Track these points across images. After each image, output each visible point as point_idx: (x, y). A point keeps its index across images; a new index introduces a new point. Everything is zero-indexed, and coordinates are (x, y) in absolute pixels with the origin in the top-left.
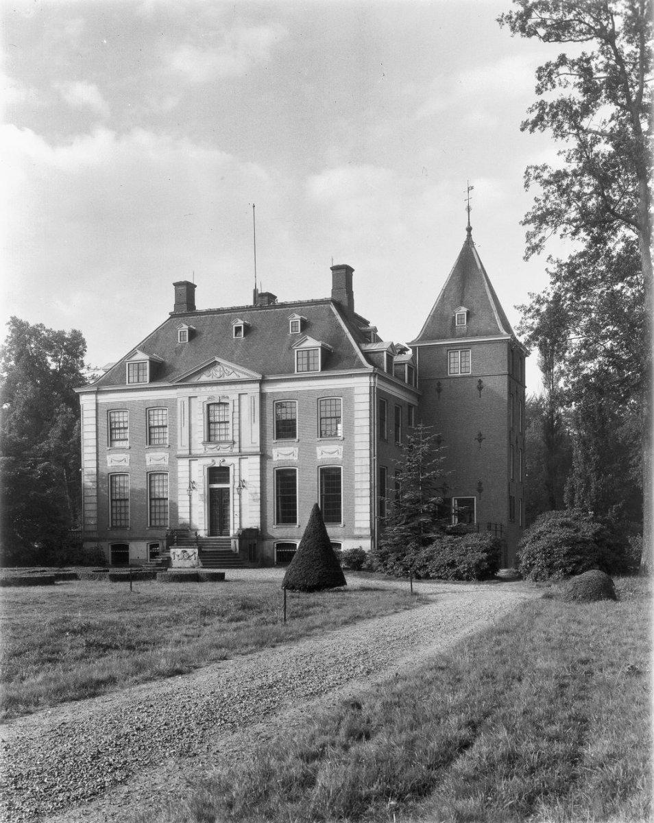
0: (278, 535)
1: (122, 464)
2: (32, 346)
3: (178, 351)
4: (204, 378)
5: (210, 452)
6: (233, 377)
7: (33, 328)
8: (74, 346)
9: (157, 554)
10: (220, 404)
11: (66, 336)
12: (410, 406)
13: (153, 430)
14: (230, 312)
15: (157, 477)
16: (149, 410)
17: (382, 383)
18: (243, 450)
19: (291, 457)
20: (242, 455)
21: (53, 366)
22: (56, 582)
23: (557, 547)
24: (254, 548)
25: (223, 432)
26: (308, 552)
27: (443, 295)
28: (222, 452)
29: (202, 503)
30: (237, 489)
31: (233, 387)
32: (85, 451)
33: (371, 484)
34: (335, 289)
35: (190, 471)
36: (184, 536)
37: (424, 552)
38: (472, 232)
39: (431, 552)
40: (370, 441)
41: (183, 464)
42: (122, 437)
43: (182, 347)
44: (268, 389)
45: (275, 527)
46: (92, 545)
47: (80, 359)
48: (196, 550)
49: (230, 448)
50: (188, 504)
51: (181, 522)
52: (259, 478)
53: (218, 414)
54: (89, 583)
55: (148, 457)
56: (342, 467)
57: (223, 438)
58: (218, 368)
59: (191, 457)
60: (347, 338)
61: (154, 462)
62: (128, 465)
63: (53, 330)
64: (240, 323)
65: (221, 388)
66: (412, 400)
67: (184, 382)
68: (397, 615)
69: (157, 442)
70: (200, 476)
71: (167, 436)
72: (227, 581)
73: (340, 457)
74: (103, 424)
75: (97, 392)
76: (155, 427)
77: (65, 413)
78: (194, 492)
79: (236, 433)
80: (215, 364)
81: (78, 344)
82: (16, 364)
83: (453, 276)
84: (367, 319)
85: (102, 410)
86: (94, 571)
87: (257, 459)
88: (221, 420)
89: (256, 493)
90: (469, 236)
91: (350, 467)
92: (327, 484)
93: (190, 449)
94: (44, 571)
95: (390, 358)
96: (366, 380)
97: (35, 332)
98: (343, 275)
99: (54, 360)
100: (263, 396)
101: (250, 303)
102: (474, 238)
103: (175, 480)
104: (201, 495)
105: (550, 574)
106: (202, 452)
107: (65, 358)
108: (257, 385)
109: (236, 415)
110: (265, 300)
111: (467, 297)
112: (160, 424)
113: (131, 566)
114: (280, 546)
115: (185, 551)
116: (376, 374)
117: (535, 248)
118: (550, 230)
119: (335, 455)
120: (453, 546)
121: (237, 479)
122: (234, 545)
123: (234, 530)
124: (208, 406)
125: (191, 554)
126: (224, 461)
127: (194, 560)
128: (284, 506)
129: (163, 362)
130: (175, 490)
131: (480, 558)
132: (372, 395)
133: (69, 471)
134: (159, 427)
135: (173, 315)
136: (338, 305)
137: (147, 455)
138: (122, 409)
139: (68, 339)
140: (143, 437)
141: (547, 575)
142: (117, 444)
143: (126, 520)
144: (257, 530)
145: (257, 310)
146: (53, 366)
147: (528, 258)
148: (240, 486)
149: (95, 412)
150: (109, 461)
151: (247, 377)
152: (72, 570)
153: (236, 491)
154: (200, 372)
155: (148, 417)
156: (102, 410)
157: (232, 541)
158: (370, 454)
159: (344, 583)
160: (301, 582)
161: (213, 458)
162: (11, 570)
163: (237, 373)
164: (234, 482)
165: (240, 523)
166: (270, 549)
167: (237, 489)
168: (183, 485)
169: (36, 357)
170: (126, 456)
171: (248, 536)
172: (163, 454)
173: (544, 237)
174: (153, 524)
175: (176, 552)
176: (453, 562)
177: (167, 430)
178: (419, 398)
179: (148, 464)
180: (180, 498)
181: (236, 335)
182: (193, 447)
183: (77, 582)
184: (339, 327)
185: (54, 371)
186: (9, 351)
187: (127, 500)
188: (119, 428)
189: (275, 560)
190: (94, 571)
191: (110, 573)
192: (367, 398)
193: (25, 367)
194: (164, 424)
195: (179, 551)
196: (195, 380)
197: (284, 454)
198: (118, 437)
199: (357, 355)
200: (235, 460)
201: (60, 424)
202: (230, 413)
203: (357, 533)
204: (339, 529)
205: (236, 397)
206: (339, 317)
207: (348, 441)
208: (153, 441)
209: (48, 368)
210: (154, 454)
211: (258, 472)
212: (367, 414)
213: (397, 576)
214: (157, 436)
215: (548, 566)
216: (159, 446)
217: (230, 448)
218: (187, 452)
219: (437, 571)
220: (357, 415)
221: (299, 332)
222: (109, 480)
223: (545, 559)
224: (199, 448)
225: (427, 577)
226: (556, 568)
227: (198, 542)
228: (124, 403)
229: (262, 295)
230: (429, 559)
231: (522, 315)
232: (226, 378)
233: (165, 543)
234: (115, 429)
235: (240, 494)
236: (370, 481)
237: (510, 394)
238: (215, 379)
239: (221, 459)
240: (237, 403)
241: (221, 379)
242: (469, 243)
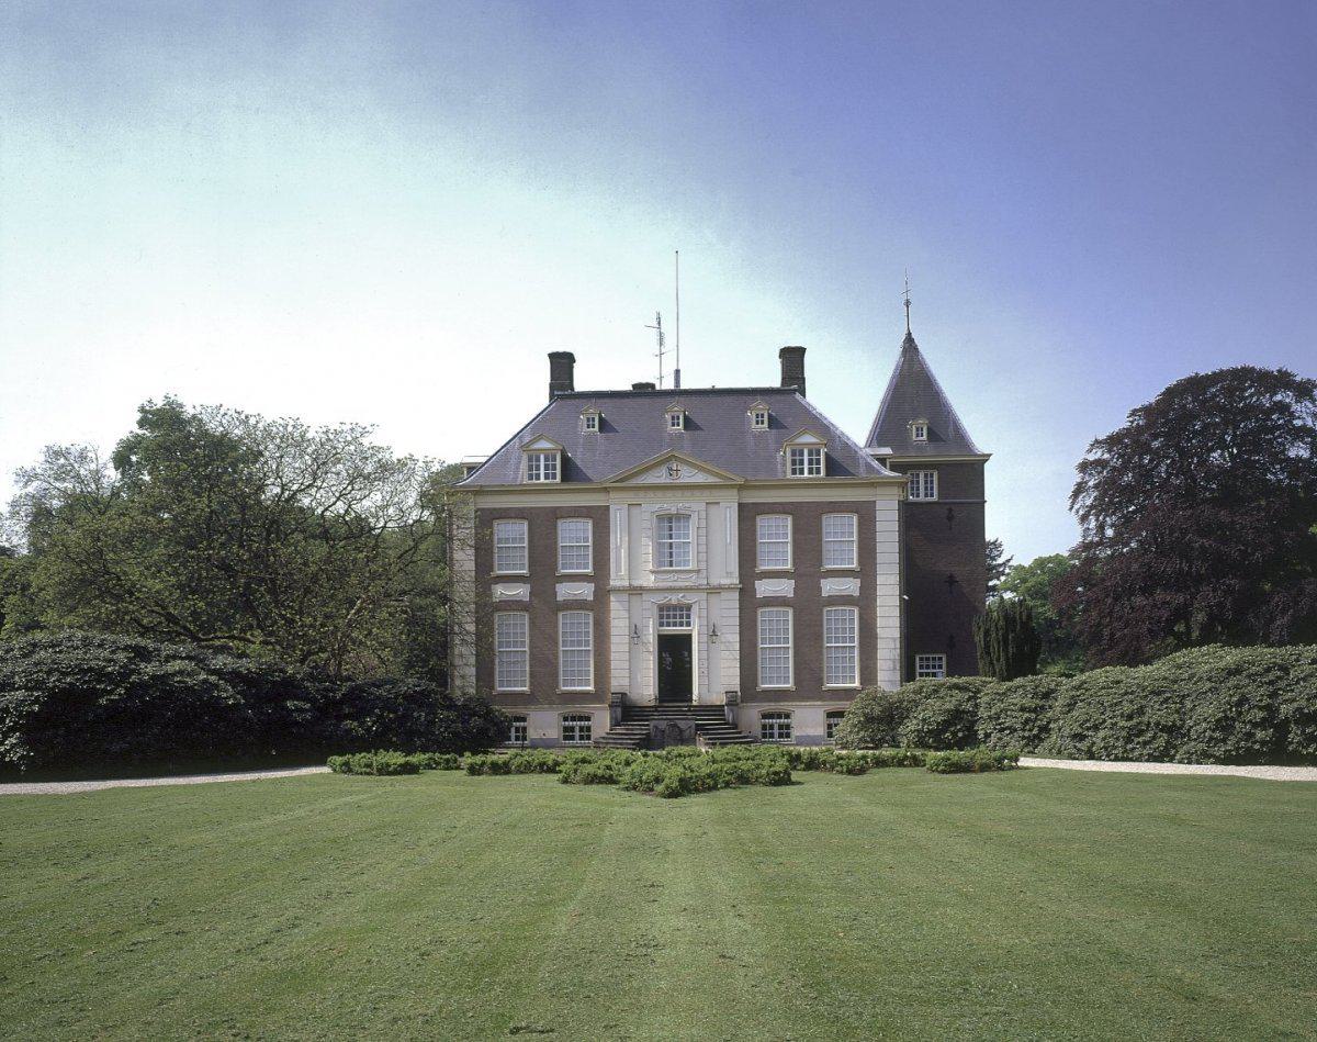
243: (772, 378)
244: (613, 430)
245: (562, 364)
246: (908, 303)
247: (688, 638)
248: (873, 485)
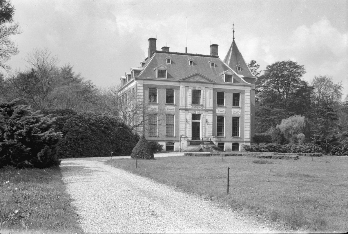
4: (206, 81)
38: (235, 39)
68: (345, 98)
70: (189, 117)
79: (204, 102)
91: (243, 118)
162: (82, 164)
196: (187, 80)
197: (220, 111)
203: (245, 140)
224: (189, 106)
241: (198, 81)
242: (234, 43)
243: (208, 53)
244: (217, 66)
245: (153, 41)
246: (234, 32)
247: (199, 123)
248: (245, 86)
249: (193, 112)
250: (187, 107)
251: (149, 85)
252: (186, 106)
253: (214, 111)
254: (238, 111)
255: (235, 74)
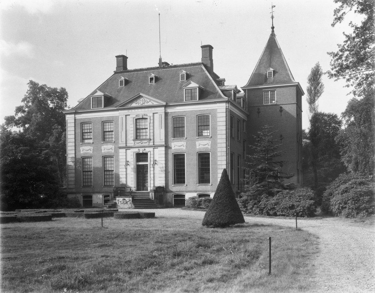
0: (174, 190)
1: (89, 152)
2: (41, 95)
3: (119, 91)
4: (134, 105)
5: (137, 145)
6: (150, 104)
7: (41, 86)
8: (62, 95)
9: (109, 200)
10: (143, 118)
11: (58, 91)
12: (244, 121)
13: (106, 134)
14: (147, 71)
15: (108, 159)
16: (104, 123)
17: (232, 107)
18: (155, 144)
19: (182, 147)
20: (155, 147)
21: (51, 105)
22: (52, 219)
23: (361, 196)
24: (162, 197)
25: (144, 134)
26: (220, 201)
27: (260, 62)
28: (144, 145)
29: (133, 173)
30: (153, 165)
31: (150, 109)
32: (68, 145)
33: (227, 162)
34: (203, 57)
35: (126, 156)
36: (123, 191)
37: (273, 200)
39: (277, 199)
40: (226, 138)
41: (122, 152)
42: (89, 137)
43: (121, 89)
44: (169, 110)
45: (198, 185)
46: (73, 196)
47: (65, 102)
48: (131, 199)
49: (148, 143)
50: (125, 173)
51: (121, 183)
52: (164, 159)
53: (142, 124)
54: (73, 220)
55: (103, 147)
56: (210, 153)
57: (144, 137)
58: (141, 99)
59: (127, 148)
60: (212, 83)
61: (106, 151)
62: (92, 152)
63: (51, 87)
64: (153, 75)
65: (143, 110)
66: (246, 119)
67: (124, 107)
69: (107, 140)
71: (113, 136)
72: (156, 218)
73: (210, 147)
74: (79, 131)
75: (75, 113)
76: (107, 132)
77: (57, 129)
78: (128, 167)
79: (152, 134)
80: (140, 97)
81: (64, 94)
82: (32, 104)
83: (265, 52)
84: (219, 76)
85: (78, 123)
86: (75, 212)
87: (163, 149)
88: (143, 127)
89: (163, 167)
90: (273, 31)
91: (215, 153)
92: (202, 162)
93: (126, 143)
94: (45, 212)
95: (235, 94)
96: (224, 105)
97: (42, 88)
98: (208, 50)
99: (52, 103)
100: (166, 114)
101: (158, 66)
102: (275, 32)
103: (117, 160)
104: (132, 168)
105: (357, 213)
106: (132, 145)
107: (57, 102)
108: (163, 108)
109: (152, 124)
110: (164, 65)
111: (274, 63)
112: (110, 130)
113: (94, 207)
114: (176, 196)
115: (125, 199)
116: (229, 101)
117: (339, 19)
118: (349, 8)
119: (207, 146)
120: (290, 196)
121: (152, 159)
122: (152, 196)
123: (150, 186)
124: (136, 120)
125: (128, 201)
126: (145, 150)
127: (130, 204)
128: (178, 174)
129: (111, 97)
130: (117, 166)
131: (310, 203)
132: (227, 113)
133: (59, 158)
134: (109, 132)
135: (116, 73)
136: (206, 66)
137: (102, 147)
138: (88, 122)
139: (58, 92)
140: (100, 137)
141: (355, 214)
142: (86, 141)
143: (91, 182)
144: (163, 187)
145: (162, 69)
146: (51, 105)
147: (334, 25)
148: (154, 163)
149: (74, 128)
150: (81, 150)
151: (158, 104)
152: (63, 211)
153: (151, 166)
154: (132, 101)
155: (103, 128)
156: (78, 123)
157: (150, 194)
158: (226, 146)
159: (243, 221)
160: (217, 221)
161: (139, 148)
163: (152, 102)
164: (150, 161)
165: (154, 184)
166: (170, 197)
167: (153, 165)
168: (122, 163)
169: (43, 100)
170: (92, 148)
171: (159, 191)
172: (111, 146)
173: (344, 13)
174: (106, 184)
175: (119, 200)
176: (293, 206)
177: (113, 133)
178: (248, 116)
179: (103, 151)
180: (120, 170)
181: (150, 83)
182: (128, 142)
183: (65, 218)
184: (207, 77)
185: (52, 108)
186: (29, 98)
187: (92, 171)
188: (87, 133)
189: (173, 203)
190: (75, 212)
191: (85, 213)
192: (224, 115)
193: (36, 106)
194: (112, 130)
195: (121, 199)
197: (177, 146)
198: (86, 137)
199: (218, 92)
200: (151, 149)
201: (55, 134)
202: (148, 124)
204: (209, 186)
205: (152, 115)
206: (206, 72)
207: (213, 137)
208: (105, 139)
209: (48, 106)
210: (106, 146)
211: (164, 156)
212: (224, 123)
213: (255, 214)
214: (107, 136)
215: (356, 209)
216: (110, 142)
217: (148, 143)
218: (125, 145)
219: (282, 212)
220: (219, 124)
221: (185, 80)
222: (81, 161)
223: (355, 204)
224: (131, 143)
225: (275, 215)
226: (361, 210)
227: (131, 194)
228: (90, 119)
229: (163, 63)
230: (276, 204)
231: (332, 58)
232: (146, 104)
233: (113, 195)
234: (85, 133)
235: (154, 168)
236: (226, 160)
237: (297, 115)
238: (140, 105)
239: (143, 149)
240: (152, 118)
241: (143, 105)
242: (273, 35)
246: (272, 17)
249: (136, 150)
250: (128, 145)
251: (81, 119)
252: (126, 143)
253: (167, 147)
254: (89, 149)
255: (218, 86)
